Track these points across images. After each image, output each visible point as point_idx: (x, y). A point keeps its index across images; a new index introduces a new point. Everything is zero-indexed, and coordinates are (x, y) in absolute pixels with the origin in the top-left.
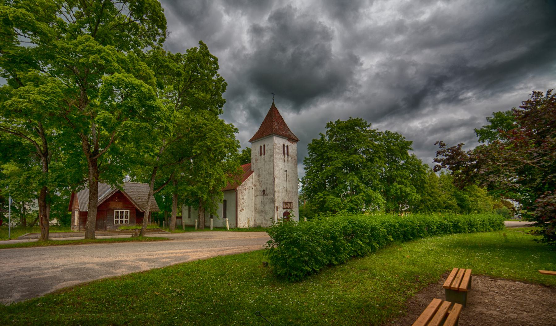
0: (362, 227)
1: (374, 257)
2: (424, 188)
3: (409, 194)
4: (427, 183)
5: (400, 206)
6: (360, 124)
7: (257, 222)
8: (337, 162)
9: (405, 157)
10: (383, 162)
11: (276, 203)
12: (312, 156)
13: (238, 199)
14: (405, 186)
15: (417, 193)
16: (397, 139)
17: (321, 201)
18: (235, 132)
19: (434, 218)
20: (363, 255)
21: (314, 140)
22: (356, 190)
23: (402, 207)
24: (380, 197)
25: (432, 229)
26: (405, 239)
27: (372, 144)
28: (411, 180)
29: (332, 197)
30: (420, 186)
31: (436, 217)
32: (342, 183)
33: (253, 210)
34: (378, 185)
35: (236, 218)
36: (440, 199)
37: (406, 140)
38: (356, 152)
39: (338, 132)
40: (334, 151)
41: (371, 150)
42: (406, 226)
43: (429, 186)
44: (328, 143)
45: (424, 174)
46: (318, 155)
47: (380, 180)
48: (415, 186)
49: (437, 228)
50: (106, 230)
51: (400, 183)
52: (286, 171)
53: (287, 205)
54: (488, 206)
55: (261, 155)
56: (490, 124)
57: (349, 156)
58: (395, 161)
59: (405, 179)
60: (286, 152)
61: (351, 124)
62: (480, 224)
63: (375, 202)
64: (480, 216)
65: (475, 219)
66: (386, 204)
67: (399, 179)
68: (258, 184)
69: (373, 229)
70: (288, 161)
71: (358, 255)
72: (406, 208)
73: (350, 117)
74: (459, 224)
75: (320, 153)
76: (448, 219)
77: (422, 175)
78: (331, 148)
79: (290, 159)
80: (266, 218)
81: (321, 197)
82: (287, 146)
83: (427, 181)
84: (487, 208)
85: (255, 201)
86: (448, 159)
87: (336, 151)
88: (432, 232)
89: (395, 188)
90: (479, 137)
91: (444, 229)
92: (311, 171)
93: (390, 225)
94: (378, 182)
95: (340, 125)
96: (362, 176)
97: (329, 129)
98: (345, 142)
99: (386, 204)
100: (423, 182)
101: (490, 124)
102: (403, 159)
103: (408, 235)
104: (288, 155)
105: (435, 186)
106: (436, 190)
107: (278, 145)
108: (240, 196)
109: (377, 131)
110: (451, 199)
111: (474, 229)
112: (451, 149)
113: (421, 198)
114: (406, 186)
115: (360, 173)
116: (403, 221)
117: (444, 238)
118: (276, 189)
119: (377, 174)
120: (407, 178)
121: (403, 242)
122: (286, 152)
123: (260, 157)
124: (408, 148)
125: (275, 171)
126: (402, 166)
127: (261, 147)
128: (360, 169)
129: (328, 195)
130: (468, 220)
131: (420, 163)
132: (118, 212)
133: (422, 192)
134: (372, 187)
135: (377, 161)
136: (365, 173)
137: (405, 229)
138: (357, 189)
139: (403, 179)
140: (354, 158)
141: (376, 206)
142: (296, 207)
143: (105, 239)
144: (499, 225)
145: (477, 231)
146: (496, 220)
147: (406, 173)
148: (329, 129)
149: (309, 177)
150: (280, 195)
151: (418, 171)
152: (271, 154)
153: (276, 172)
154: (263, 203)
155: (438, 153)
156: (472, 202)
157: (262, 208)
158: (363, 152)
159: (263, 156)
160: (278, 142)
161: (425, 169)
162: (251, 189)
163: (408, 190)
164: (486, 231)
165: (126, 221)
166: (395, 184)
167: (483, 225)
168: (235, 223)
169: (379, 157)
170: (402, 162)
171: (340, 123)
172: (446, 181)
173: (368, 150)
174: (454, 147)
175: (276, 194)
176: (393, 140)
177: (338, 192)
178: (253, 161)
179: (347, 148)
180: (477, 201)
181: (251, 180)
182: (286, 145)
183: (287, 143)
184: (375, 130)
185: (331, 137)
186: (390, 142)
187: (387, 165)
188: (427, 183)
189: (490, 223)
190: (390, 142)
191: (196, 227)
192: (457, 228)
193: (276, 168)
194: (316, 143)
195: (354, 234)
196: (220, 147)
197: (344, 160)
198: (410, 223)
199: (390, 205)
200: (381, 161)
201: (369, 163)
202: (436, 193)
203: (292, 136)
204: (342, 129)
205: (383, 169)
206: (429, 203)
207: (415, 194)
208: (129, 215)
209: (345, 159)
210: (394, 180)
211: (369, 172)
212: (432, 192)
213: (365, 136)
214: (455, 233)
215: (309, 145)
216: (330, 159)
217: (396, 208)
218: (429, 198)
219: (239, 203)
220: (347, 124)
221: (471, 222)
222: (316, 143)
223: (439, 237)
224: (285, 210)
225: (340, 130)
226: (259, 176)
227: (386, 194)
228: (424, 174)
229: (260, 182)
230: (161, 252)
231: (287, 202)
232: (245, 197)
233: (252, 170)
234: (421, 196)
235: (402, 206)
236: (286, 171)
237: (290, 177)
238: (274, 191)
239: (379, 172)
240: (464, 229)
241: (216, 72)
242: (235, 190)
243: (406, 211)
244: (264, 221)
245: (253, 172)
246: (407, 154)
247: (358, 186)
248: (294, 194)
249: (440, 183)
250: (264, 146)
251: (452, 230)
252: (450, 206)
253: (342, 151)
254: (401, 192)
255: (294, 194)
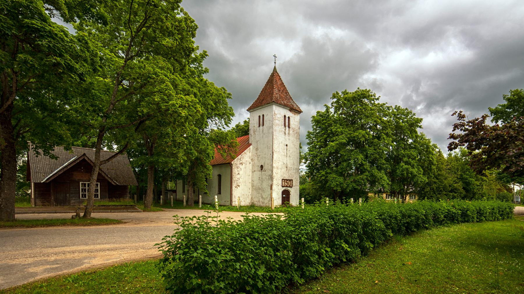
0: (349, 223)
1: (364, 262)
2: (431, 170)
3: (416, 175)
4: (435, 165)
5: (406, 187)
6: (369, 96)
7: (254, 200)
8: (341, 137)
9: (414, 135)
10: (391, 139)
11: (274, 180)
12: (316, 130)
13: (233, 174)
14: (412, 166)
15: (424, 174)
16: (407, 115)
17: (323, 180)
18: (228, 97)
19: (441, 206)
20: (350, 261)
21: (318, 112)
22: (360, 169)
23: (408, 189)
24: (385, 178)
25: (438, 218)
26: (408, 232)
27: (380, 119)
28: (418, 160)
29: (335, 176)
30: (428, 167)
31: (444, 205)
32: (345, 161)
33: (250, 186)
34: (384, 164)
35: (231, 194)
36: (446, 182)
37: (416, 117)
38: (363, 127)
39: (345, 104)
40: (338, 125)
41: (378, 126)
42: (409, 217)
43: (436, 168)
44: (333, 116)
45: (432, 155)
46: (322, 129)
47: (387, 160)
48: (422, 167)
49: (445, 217)
50: (69, 204)
51: (407, 163)
52: (287, 145)
53: (287, 182)
54: (492, 191)
55: (259, 126)
56: (505, 103)
57: (354, 131)
58: (403, 139)
59: (413, 159)
60: (287, 124)
61: (359, 95)
62: (489, 213)
63: (379, 183)
64: (489, 202)
65: (485, 207)
66: (391, 185)
67: (405, 159)
68: (256, 158)
69: (366, 225)
70: (289, 134)
71: (342, 262)
72: (411, 190)
73: (358, 88)
74: (468, 212)
75: (324, 126)
76: (457, 207)
77: (431, 155)
78: (335, 121)
79: (291, 132)
80: (264, 196)
81: (323, 175)
82: (289, 118)
83: (435, 162)
84: (491, 192)
85: (252, 177)
86: (467, 135)
87: (341, 125)
88: (438, 222)
89: (401, 169)
90: (493, 116)
91: (451, 219)
92: (314, 147)
93: (390, 217)
94: (384, 161)
95: (346, 96)
96: (367, 153)
97: (335, 100)
98: (351, 116)
99: (391, 185)
100: (431, 163)
101: (505, 103)
102: (412, 138)
103: (410, 226)
104: (289, 127)
105: (442, 168)
106: (443, 172)
107: (278, 116)
108: (235, 171)
109: (387, 105)
110: (456, 183)
111: (483, 218)
112: (473, 122)
113: (427, 181)
114: (413, 166)
115: (366, 150)
116: (406, 210)
117: (452, 229)
118: (274, 165)
119: (383, 152)
120: (414, 159)
121: (404, 236)
122: (287, 124)
123: (258, 128)
124: (418, 126)
125: (274, 145)
126: (410, 145)
127: (260, 117)
128: (367, 146)
129: (330, 173)
130: (478, 208)
131: (429, 142)
132: (85, 184)
133: (429, 174)
134: (377, 167)
135: (384, 138)
136: (371, 151)
137: (408, 220)
138: (362, 168)
139: (410, 160)
140: (359, 133)
141: (380, 187)
142: (296, 185)
143: (38, 220)
144: (508, 214)
145: (486, 220)
146: (506, 209)
147: (414, 153)
148: (335, 100)
149: (312, 153)
150: (279, 171)
151: (427, 151)
152: (270, 125)
153: (275, 147)
154: (261, 180)
155: (456, 127)
156: (478, 186)
157: (259, 185)
158: (370, 128)
159: (261, 127)
160: (278, 112)
161: (433, 150)
162: (248, 163)
163: (415, 171)
164: (494, 220)
165: (96, 196)
166: (402, 164)
167: (492, 214)
168: (229, 200)
169: (387, 134)
170: (410, 141)
171: (347, 93)
172: (453, 163)
173: (376, 126)
174: (477, 120)
175: (275, 170)
176: (403, 116)
177: (341, 171)
178: (251, 132)
179: (353, 123)
180: (482, 186)
181: (248, 153)
182: (287, 116)
183: (289, 114)
184: (384, 104)
185: (337, 109)
186: (399, 119)
187: (395, 143)
188: (435, 165)
189: (499, 212)
190: (399, 119)
191: (185, 203)
192: (465, 217)
193: (275, 142)
194: (320, 115)
195: (336, 234)
196: (173, 105)
197: (349, 136)
198: (415, 213)
199: (396, 187)
200: (388, 138)
201: (376, 140)
202: (442, 175)
203: (295, 106)
204: (348, 101)
205: (391, 148)
206: (434, 186)
207: (421, 176)
208: (99, 188)
209: (350, 134)
210: (401, 159)
211: (375, 150)
212: (439, 174)
213: (373, 110)
214: (462, 222)
215: (313, 117)
216: (334, 134)
217: (401, 190)
218: (435, 180)
219: (234, 179)
220: (354, 95)
221: (480, 210)
222: (320, 115)
223: (446, 229)
224: (284, 188)
225: (346, 102)
226: (257, 149)
227: (392, 175)
228: (432, 155)
229: (258, 156)
230: (68, 249)
231: (287, 180)
232: (241, 173)
233: (250, 143)
234: (428, 178)
235: (407, 188)
236: (287, 145)
237: (291, 152)
238: (272, 167)
239: (386, 151)
240: (473, 218)
241: (179, 7)
242: (230, 165)
243: (411, 192)
244: (261, 200)
245: (251, 144)
246: (416, 133)
247: (362, 165)
248: (294, 171)
249: (447, 165)
250: (263, 115)
251: (460, 219)
252: (456, 189)
253: (347, 125)
254: (407, 174)
255: (294, 171)
